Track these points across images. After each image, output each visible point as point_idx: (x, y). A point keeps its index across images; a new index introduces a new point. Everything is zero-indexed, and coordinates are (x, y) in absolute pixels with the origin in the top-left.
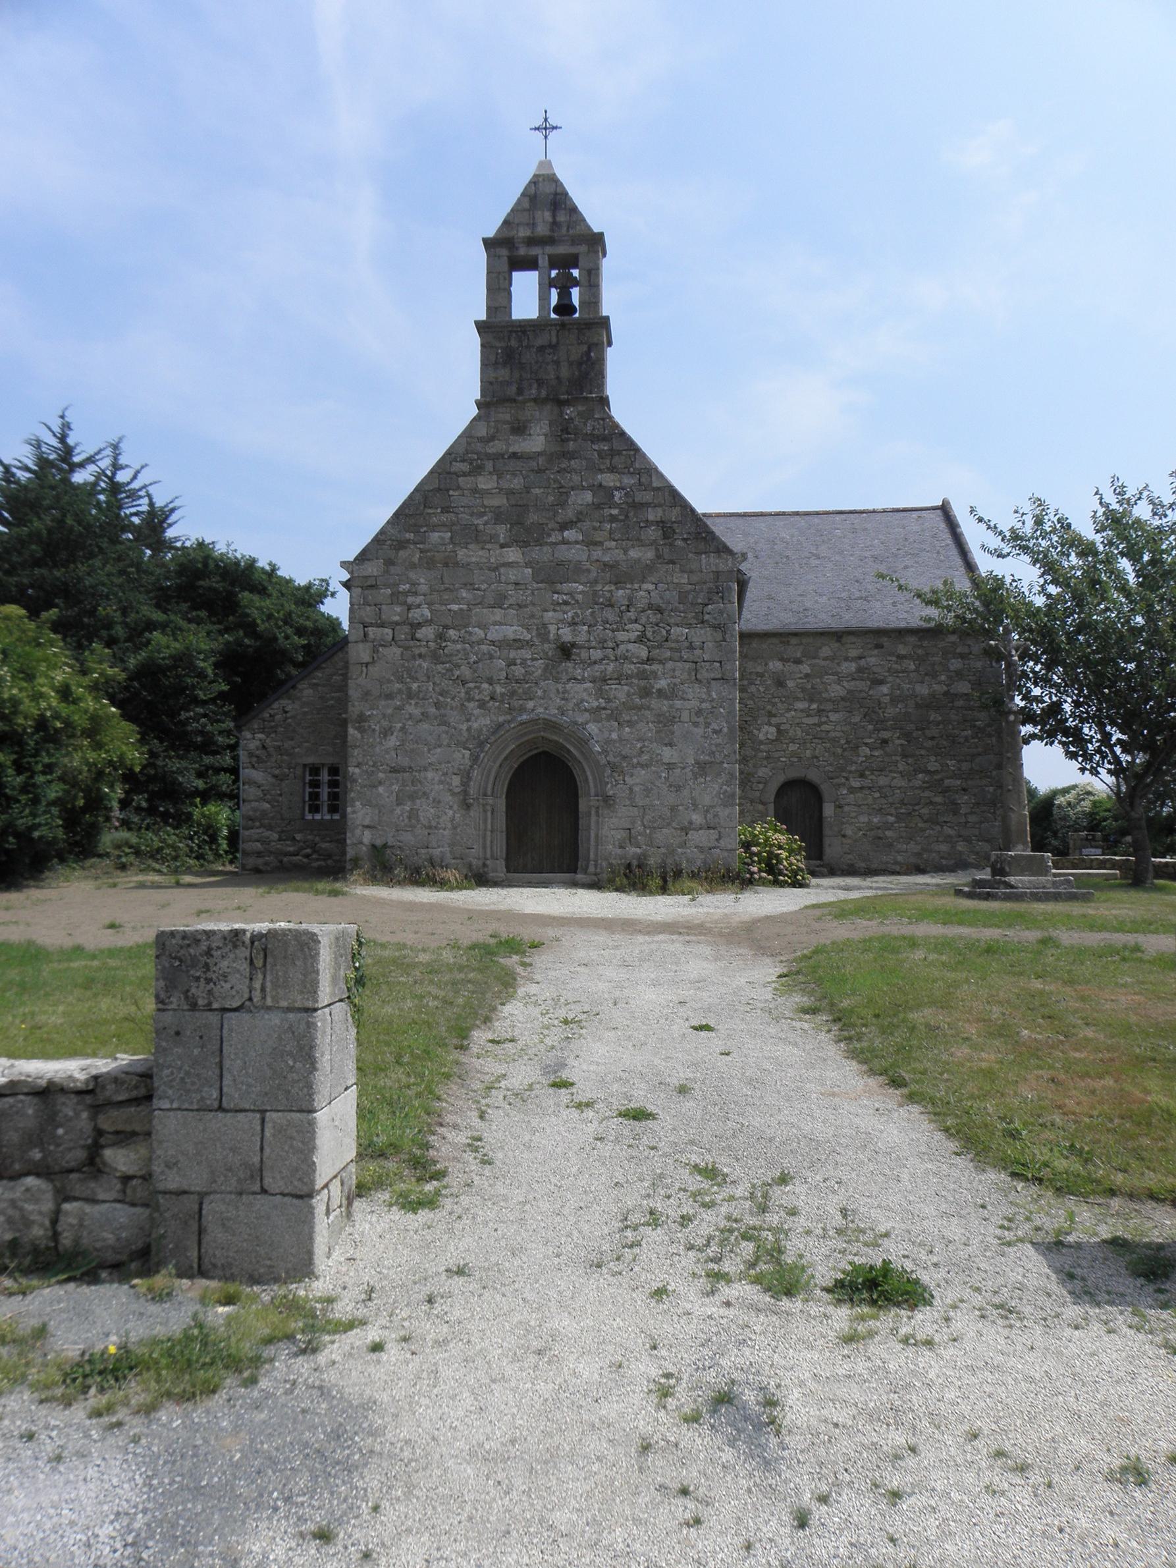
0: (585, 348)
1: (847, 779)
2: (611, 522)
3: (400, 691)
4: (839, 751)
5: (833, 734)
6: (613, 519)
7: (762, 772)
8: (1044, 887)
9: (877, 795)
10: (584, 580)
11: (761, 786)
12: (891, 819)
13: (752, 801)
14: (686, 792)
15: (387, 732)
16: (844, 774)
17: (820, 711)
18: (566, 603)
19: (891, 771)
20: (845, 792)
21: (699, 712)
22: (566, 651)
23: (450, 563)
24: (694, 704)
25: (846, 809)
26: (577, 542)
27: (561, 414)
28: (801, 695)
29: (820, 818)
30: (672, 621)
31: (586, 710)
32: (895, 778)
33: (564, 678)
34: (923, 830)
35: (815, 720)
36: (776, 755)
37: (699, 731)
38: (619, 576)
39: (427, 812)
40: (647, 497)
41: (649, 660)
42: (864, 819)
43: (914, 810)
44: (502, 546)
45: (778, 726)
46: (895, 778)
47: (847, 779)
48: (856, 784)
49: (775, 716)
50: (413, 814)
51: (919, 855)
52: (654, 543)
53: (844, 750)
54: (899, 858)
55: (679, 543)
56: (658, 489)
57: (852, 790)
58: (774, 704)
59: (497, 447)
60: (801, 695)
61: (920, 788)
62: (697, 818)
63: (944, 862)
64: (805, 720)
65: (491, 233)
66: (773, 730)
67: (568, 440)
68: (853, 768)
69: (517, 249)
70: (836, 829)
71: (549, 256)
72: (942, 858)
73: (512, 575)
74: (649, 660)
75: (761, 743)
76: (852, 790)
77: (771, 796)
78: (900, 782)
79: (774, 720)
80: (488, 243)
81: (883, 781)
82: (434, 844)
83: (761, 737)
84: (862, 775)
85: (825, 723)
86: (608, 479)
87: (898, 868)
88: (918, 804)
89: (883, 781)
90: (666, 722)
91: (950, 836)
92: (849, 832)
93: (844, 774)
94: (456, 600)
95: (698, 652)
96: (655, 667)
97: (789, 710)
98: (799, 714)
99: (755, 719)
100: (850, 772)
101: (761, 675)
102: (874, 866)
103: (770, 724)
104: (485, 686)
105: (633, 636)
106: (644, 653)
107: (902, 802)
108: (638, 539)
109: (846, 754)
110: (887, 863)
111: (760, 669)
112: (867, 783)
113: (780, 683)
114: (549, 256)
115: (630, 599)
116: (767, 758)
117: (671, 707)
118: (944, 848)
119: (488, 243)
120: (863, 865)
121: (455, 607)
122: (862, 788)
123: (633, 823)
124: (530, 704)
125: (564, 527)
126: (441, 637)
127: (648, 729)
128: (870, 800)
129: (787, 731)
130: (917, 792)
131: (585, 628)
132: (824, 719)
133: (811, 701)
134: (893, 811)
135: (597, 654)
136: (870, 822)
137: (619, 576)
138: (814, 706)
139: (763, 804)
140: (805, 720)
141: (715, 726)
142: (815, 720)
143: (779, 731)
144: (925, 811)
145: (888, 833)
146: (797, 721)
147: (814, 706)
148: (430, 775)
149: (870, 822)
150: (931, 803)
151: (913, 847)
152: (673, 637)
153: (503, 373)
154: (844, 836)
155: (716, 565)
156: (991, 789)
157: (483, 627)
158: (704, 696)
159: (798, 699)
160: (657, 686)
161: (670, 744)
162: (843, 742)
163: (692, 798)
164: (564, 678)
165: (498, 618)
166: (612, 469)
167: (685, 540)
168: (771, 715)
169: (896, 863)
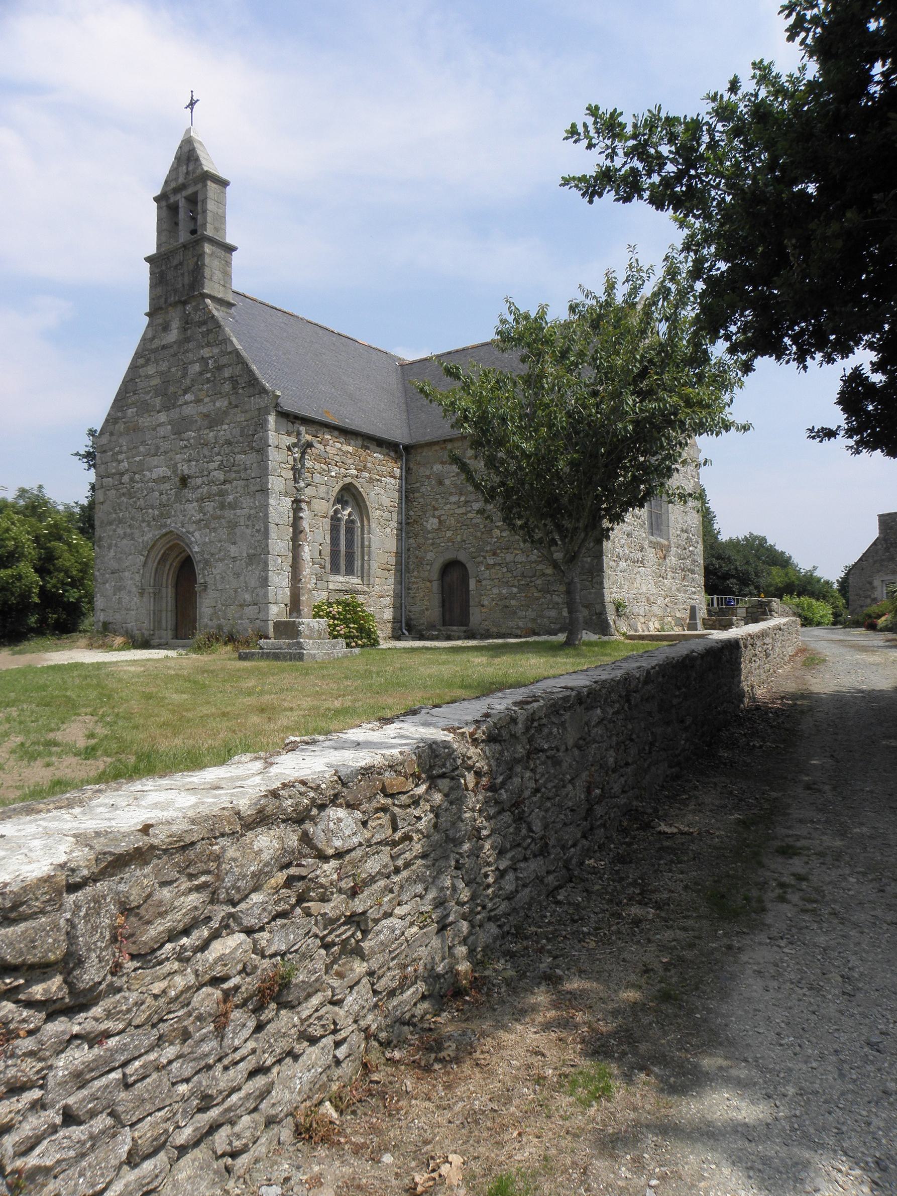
0: (195, 259)
1: (485, 558)
2: (207, 383)
3: (115, 520)
4: (479, 534)
5: (474, 521)
6: (208, 381)
7: (430, 556)
8: (280, 649)
9: (505, 570)
10: (194, 429)
11: (428, 567)
12: (515, 590)
13: (423, 580)
14: (242, 578)
15: (110, 547)
16: (482, 554)
17: (466, 502)
18: (186, 447)
19: (515, 549)
20: (483, 569)
21: (249, 518)
22: (184, 481)
23: (136, 429)
24: (246, 511)
25: (484, 583)
26: (191, 402)
27: (185, 310)
28: (453, 490)
29: (467, 591)
30: (236, 450)
31: (194, 522)
32: (517, 554)
33: (184, 500)
34: (538, 599)
35: (463, 510)
36: (438, 541)
37: (249, 531)
38: (213, 421)
39: (126, 599)
40: (224, 360)
41: (225, 482)
42: (496, 591)
43: (531, 582)
44: (158, 412)
45: (439, 517)
46: (517, 554)
47: (485, 558)
48: (491, 562)
49: (437, 509)
50: (120, 601)
51: (534, 620)
52: (228, 394)
53: (483, 533)
54: (521, 624)
55: (240, 391)
56: (230, 353)
57: (488, 567)
58: (437, 500)
59: (157, 343)
60: (453, 490)
61: (535, 562)
62: (247, 597)
63: (553, 626)
64: (457, 511)
65: (158, 192)
66: (436, 521)
67: (188, 328)
68: (488, 548)
69: (169, 198)
70: (477, 600)
71: (185, 198)
72: (551, 623)
73: (162, 431)
74: (225, 482)
75: (429, 532)
76: (488, 567)
77: (435, 575)
78: (521, 558)
79: (437, 513)
80: (156, 199)
81: (509, 558)
82: (129, 621)
83: (429, 527)
84: (495, 554)
85: (470, 512)
86: (206, 352)
87: (519, 632)
88: (534, 576)
89: (509, 558)
90: (233, 525)
91: (557, 604)
92: (486, 603)
93: (482, 554)
94: (138, 455)
95: (249, 471)
96: (228, 486)
97: (447, 503)
98: (453, 507)
99: (425, 512)
100: (487, 551)
101: (428, 477)
102: (503, 631)
103: (434, 516)
104: (150, 511)
105: (216, 465)
106: (222, 477)
107: (523, 576)
108: (221, 393)
109: (484, 536)
110: (512, 628)
111: (428, 473)
112: (498, 560)
113: (441, 483)
114: (185, 198)
115: (216, 438)
116: (433, 544)
117: (235, 515)
118: (553, 613)
119: (156, 199)
120: (495, 630)
121: (137, 459)
122: (494, 565)
123: (217, 602)
124: (169, 521)
125: (185, 392)
126: (132, 480)
127: (223, 533)
128: (500, 576)
129: (445, 521)
130: (533, 565)
131: (194, 463)
132: (469, 509)
133: (461, 494)
134: (516, 583)
135: (199, 481)
136: (500, 593)
137: (213, 421)
138: (463, 499)
139: (430, 581)
140: (457, 511)
141: (257, 527)
142: (463, 510)
143: (440, 522)
144: (539, 582)
145: (513, 602)
146: (452, 512)
147: (463, 499)
148: (126, 574)
149: (500, 593)
150: (544, 575)
151: (531, 614)
152: (237, 463)
153: (159, 290)
154: (483, 606)
155: (259, 404)
156: (589, 559)
157: (150, 470)
158: (252, 505)
159: (451, 494)
160: (228, 500)
161: (234, 543)
162: (482, 526)
163: (245, 582)
164: (184, 500)
165: (156, 463)
166: (208, 344)
167: (243, 388)
168: (435, 509)
169: (518, 628)
